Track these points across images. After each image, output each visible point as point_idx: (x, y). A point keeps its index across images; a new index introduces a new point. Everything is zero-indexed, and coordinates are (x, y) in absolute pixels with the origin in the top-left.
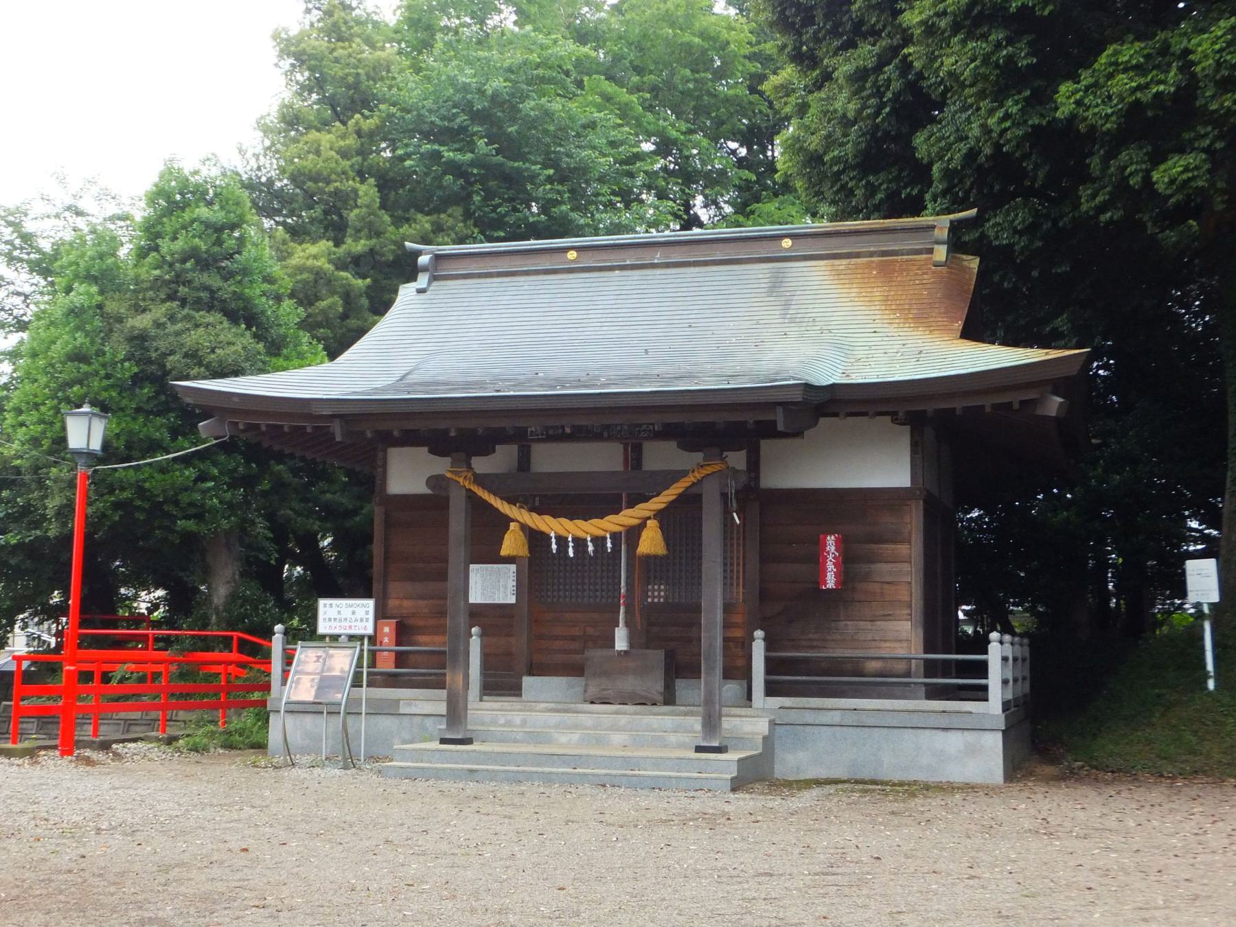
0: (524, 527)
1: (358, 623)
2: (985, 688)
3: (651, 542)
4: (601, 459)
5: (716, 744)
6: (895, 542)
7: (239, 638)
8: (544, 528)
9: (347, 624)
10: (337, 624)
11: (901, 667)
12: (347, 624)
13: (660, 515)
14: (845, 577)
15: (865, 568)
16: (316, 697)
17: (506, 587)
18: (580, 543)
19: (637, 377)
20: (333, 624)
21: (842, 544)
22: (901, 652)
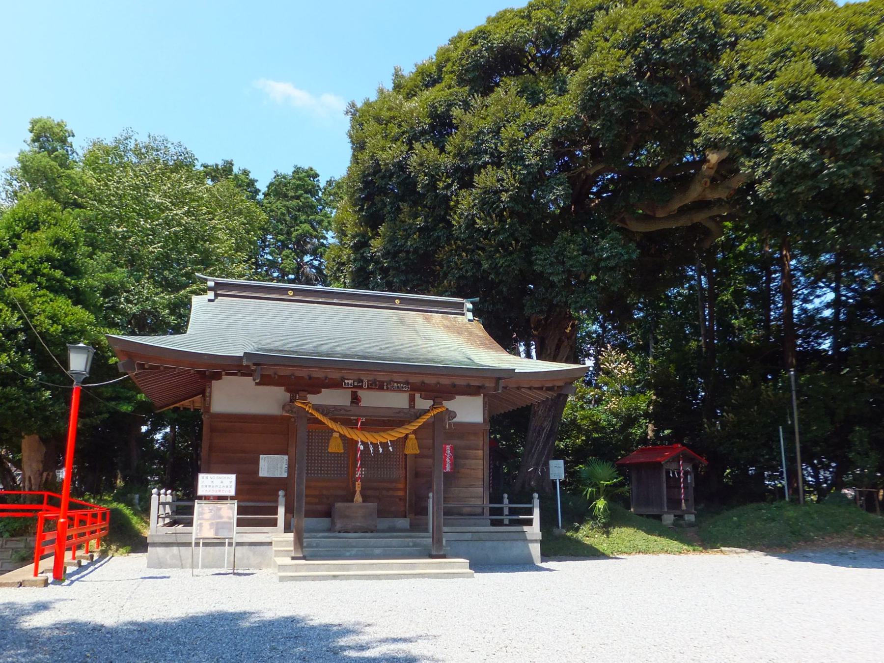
0: (342, 437)
1: (225, 489)
2: (276, 519)
3: (412, 448)
4: (398, 401)
5: (442, 553)
6: (475, 449)
7: (48, 496)
8: (355, 438)
9: (218, 489)
10: (211, 489)
11: (479, 510)
12: (218, 489)
13: (415, 432)
14: (454, 465)
15: (462, 462)
16: (216, 534)
17: (281, 468)
18: (385, 445)
19: (285, 351)
20: (208, 489)
21: (452, 449)
22: (479, 502)
